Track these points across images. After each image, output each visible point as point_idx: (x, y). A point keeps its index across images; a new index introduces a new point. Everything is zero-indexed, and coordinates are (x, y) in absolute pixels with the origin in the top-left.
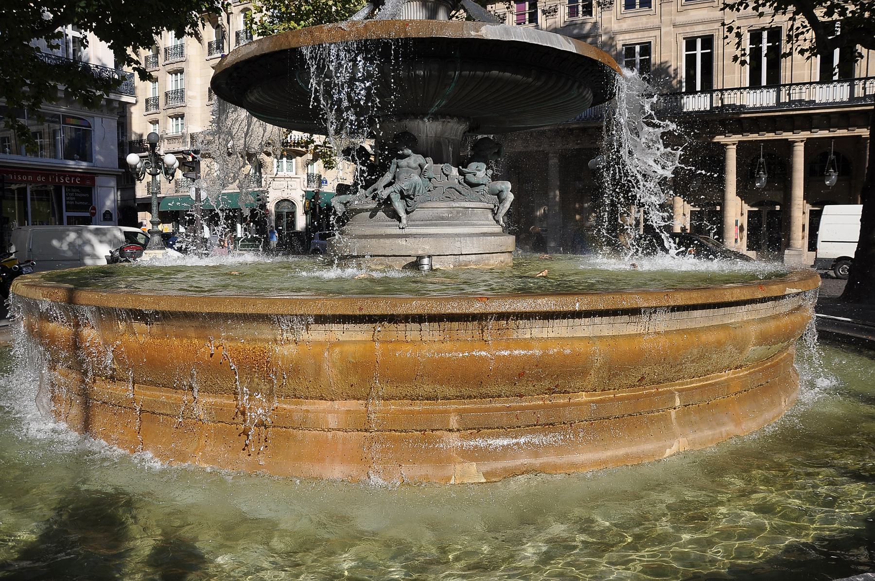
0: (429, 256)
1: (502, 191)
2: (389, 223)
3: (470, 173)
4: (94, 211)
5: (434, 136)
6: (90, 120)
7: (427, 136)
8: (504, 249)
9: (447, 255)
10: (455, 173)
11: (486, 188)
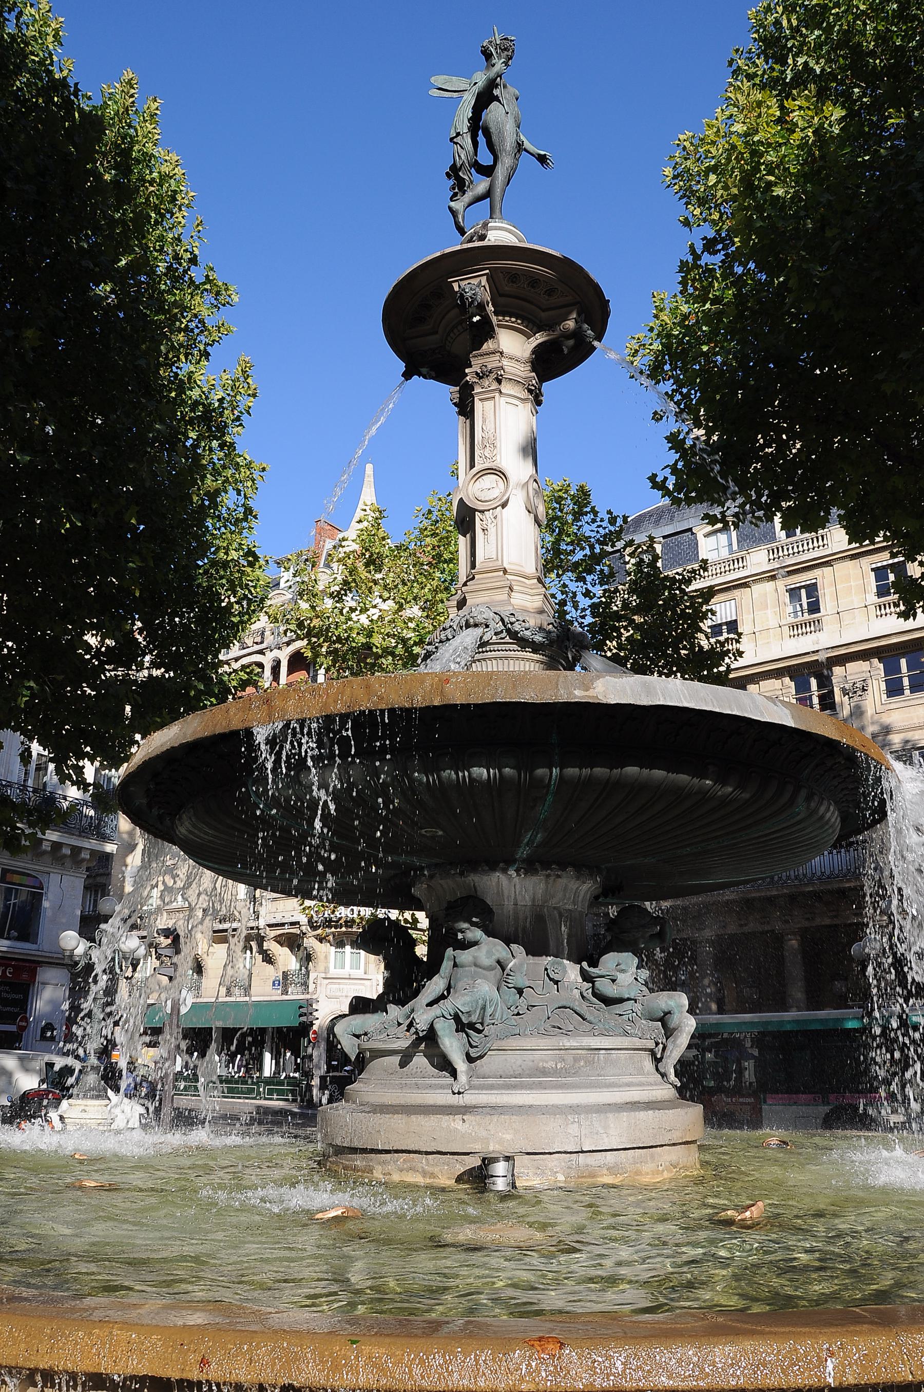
0: (507, 1159)
1: (669, 1013)
2: (434, 1081)
3: (603, 977)
4: (24, 1024)
5: (529, 903)
6: (43, 878)
7: (516, 904)
8: (676, 1137)
9: (550, 1153)
10: (573, 977)
11: (638, 1007)
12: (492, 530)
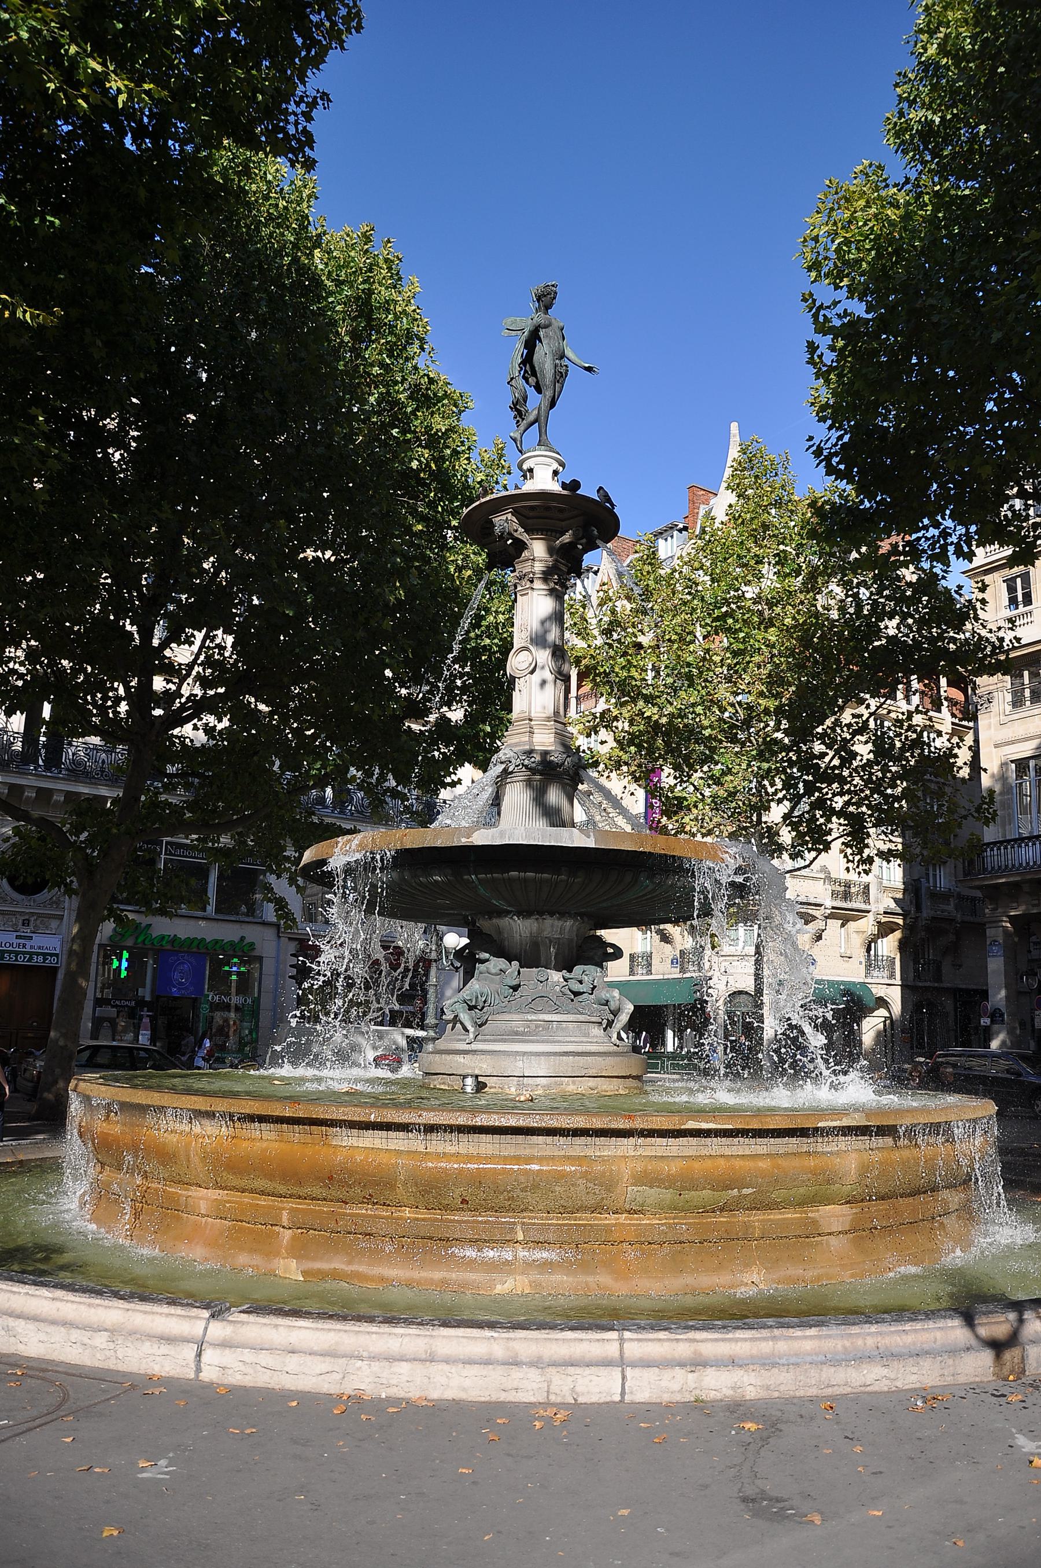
12: (525, 691)
